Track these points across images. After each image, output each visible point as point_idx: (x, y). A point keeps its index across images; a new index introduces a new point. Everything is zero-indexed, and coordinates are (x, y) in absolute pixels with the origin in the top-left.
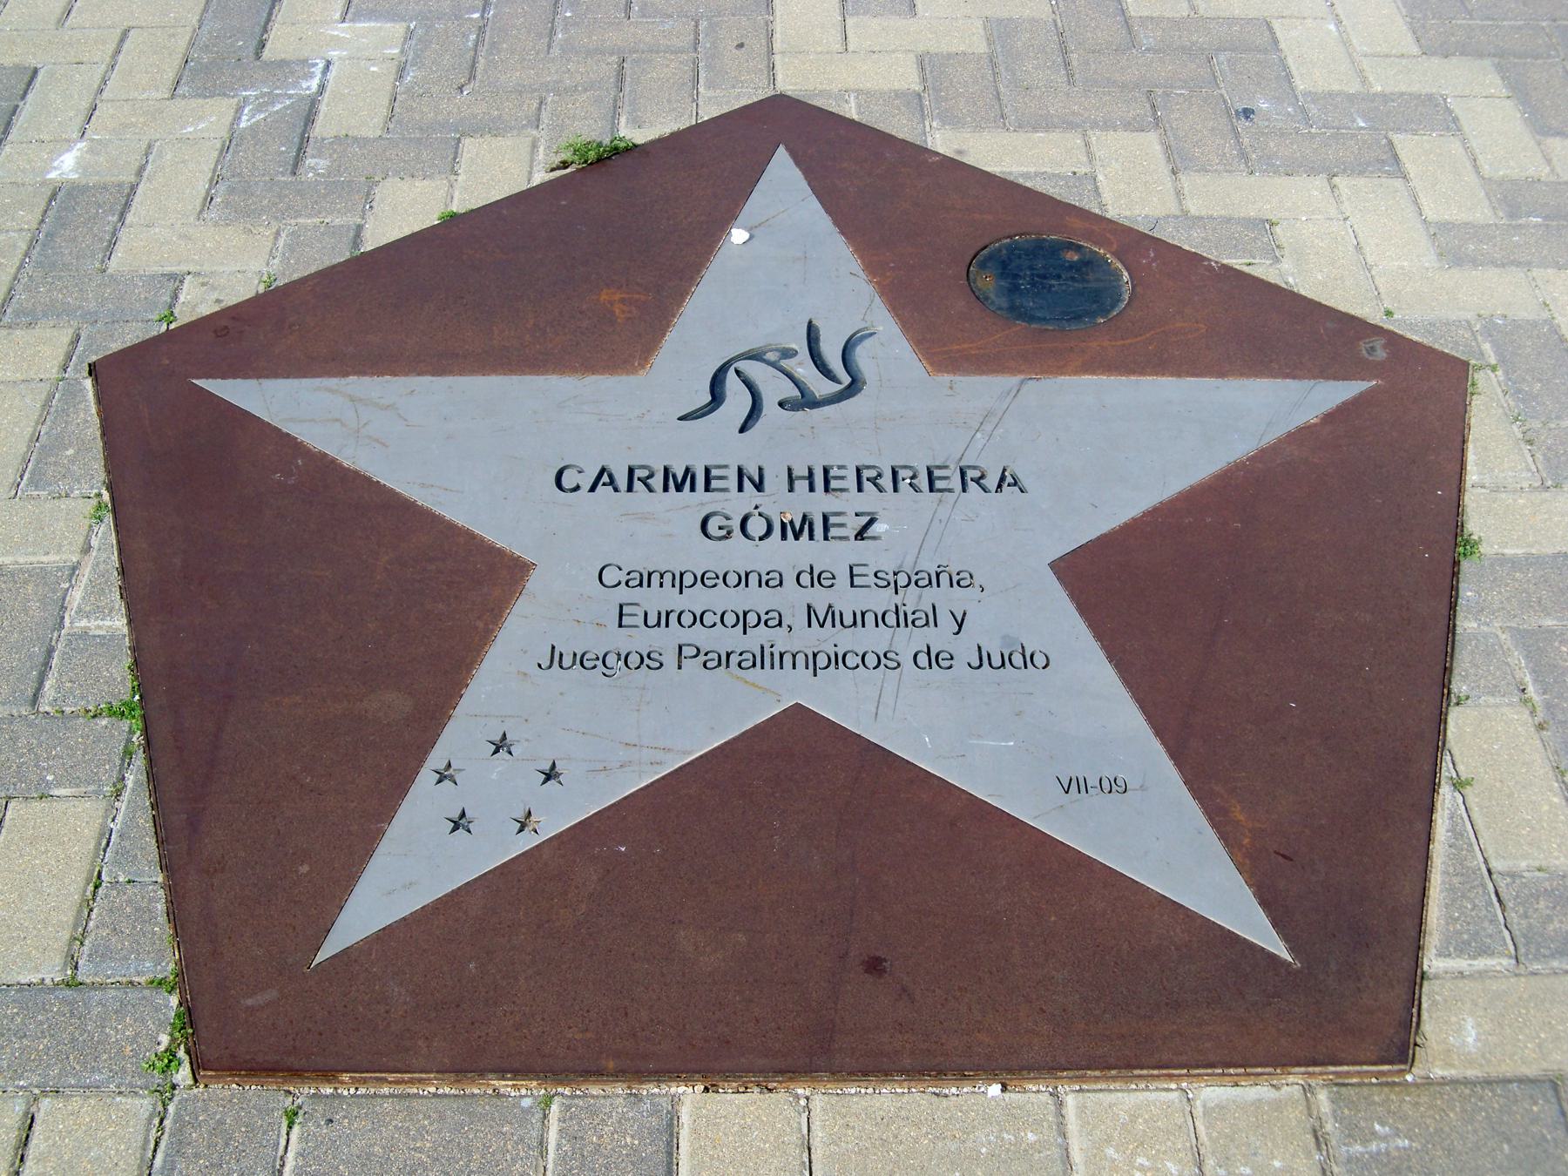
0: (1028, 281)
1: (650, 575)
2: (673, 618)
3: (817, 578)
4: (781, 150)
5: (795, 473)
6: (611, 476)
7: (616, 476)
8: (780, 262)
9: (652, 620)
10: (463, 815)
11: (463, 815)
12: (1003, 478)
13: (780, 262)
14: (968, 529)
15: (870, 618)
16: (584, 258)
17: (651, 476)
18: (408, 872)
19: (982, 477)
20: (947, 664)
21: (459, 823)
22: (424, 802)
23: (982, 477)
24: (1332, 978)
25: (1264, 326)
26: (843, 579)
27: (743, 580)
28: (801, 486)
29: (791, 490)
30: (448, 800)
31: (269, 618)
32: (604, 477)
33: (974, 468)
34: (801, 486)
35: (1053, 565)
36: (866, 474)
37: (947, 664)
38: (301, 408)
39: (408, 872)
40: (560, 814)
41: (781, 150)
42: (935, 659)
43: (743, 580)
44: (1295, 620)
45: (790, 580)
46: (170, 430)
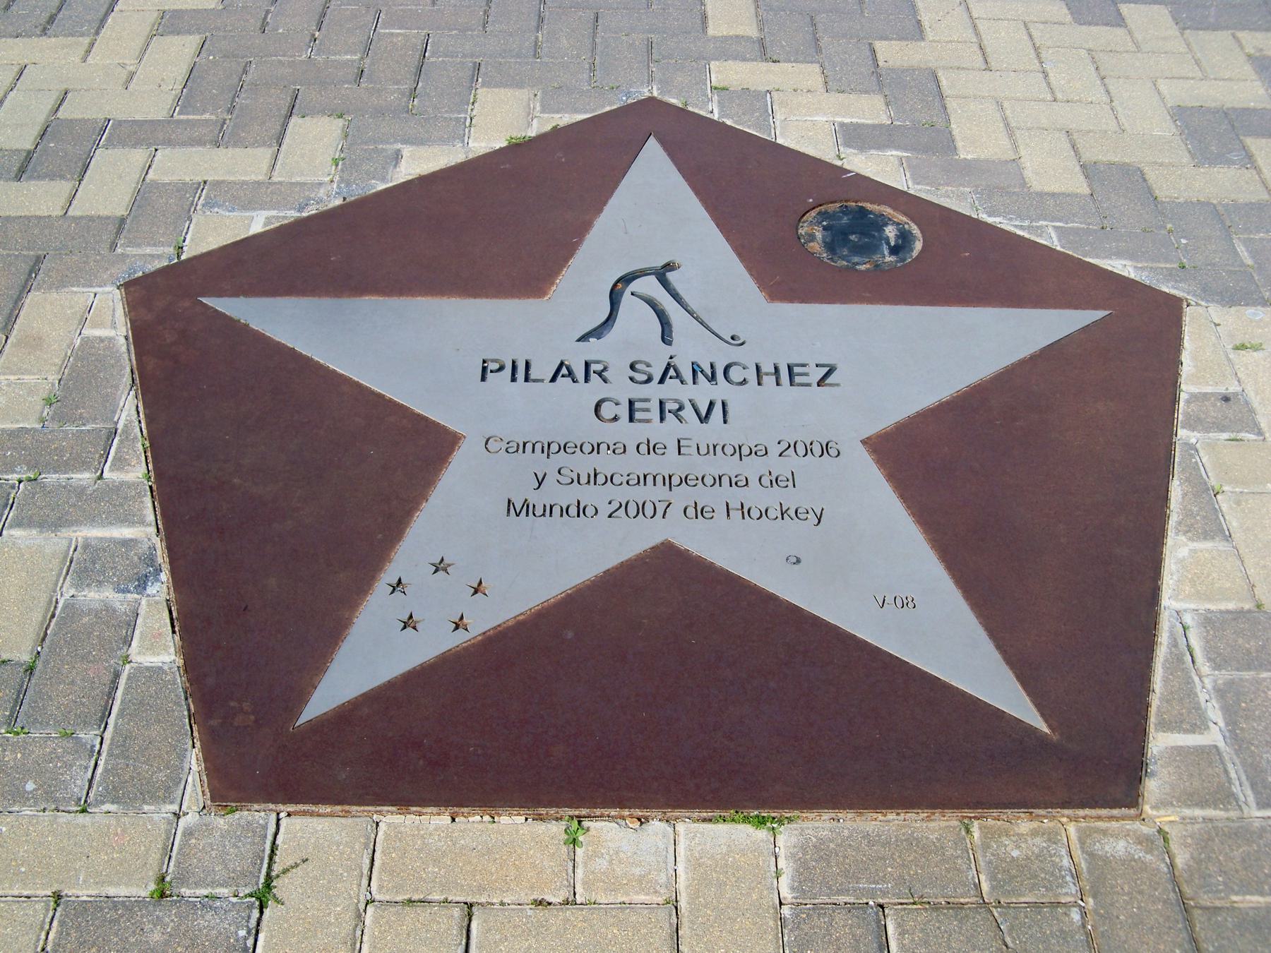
0: (818, 233)
1: (645, 477)
2: (719, 449)
3: (652, 449)
4: (652, 145)
5: (764, 369)
6: (568, 368)
7: (574, 368)
8: (653, 210)
9: (703, 450)
10: (400, 582)
11: (411, 617)
12: (667, 370)
13: (653, 210)
14: (803, 411)
15: (556, 510)
16: (493, 226)
17: (681, 409)
18: (373, 653)
19: (605, 369)
20: (709, 515)
21: (409, 623)
22: (376, 613)
23: (605, 369)
24: (1088, 747)
25: (969, 262)
26: (673, 447)
27: (596, 448)
28: (769, 381)
29: (483, 379)
30: (399, 607)
31: (262, 481)
32: (562, 371)
33: (598, 362)
34: (769, 381)
35: (864, 442)
36: (594, 367)
37: (709, 515)
38: (286, 322)
39: (373, 653)
40: (486, 617)
41: (652, 145)
42: (700, 512)
43: (596, 448)
44: (1051, 486)
45: (631, 448)
46: (187, 344)
